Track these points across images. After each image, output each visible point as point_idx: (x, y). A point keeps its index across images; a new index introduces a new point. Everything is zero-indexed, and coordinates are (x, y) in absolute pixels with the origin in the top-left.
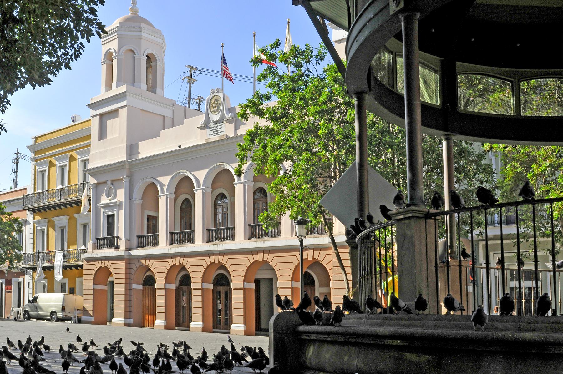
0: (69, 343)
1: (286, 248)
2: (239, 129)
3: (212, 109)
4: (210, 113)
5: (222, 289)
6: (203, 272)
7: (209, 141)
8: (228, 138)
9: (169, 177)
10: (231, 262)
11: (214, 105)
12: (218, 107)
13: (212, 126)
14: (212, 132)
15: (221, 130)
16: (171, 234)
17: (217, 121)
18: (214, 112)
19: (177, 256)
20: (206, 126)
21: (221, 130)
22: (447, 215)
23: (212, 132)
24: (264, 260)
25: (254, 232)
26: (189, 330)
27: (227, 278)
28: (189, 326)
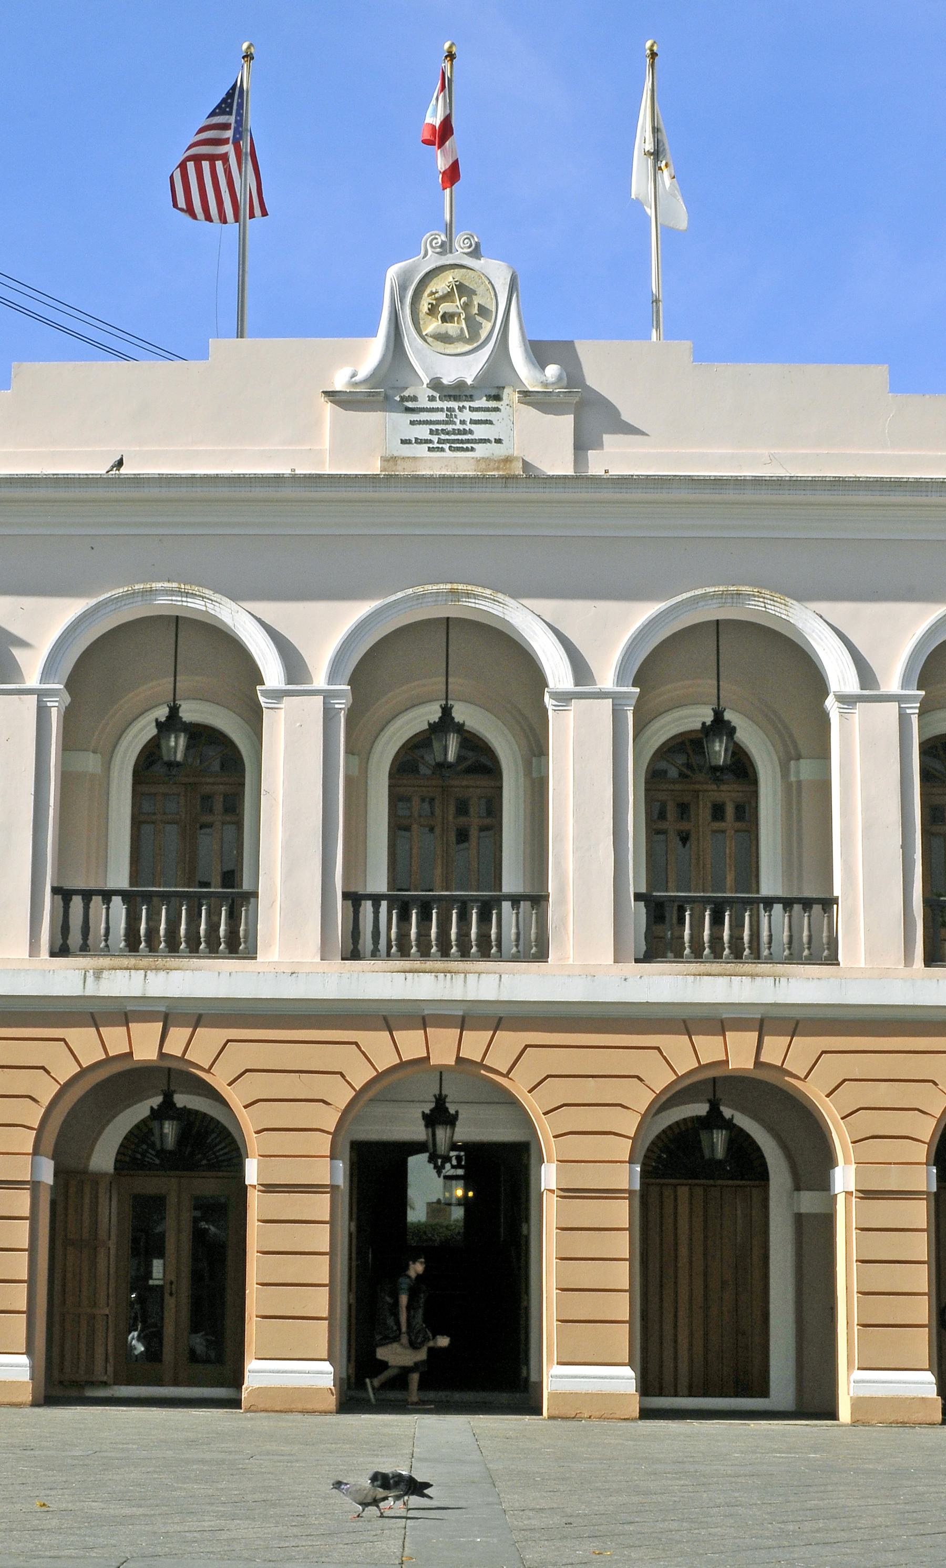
0: (370, 1473)
1: (830, 1014)
2: (599, 445)
3: (432, 326)
4: (411, 342)
5: (178, 1193)
6: (46, 1101)
7: (403, 470)
8: (532, 476)
9: (70, 609)
10: (241, 1057)
11: (444, 307)
12: (474, 327)
13: (423, 403)
14: (423, 432)
15: (480, 432)
16: (63, 894)
17: (461, 385)
18: (444, 338)
19: (146, 1017)
20: (385, 392)
21: (480, 432)
22: (758, 904)
23: (423, 432)
24: (459, 1060)
25: (660, 931)
26: (235, 1403)
27: (229, 1134)
28: (237, 1380)
